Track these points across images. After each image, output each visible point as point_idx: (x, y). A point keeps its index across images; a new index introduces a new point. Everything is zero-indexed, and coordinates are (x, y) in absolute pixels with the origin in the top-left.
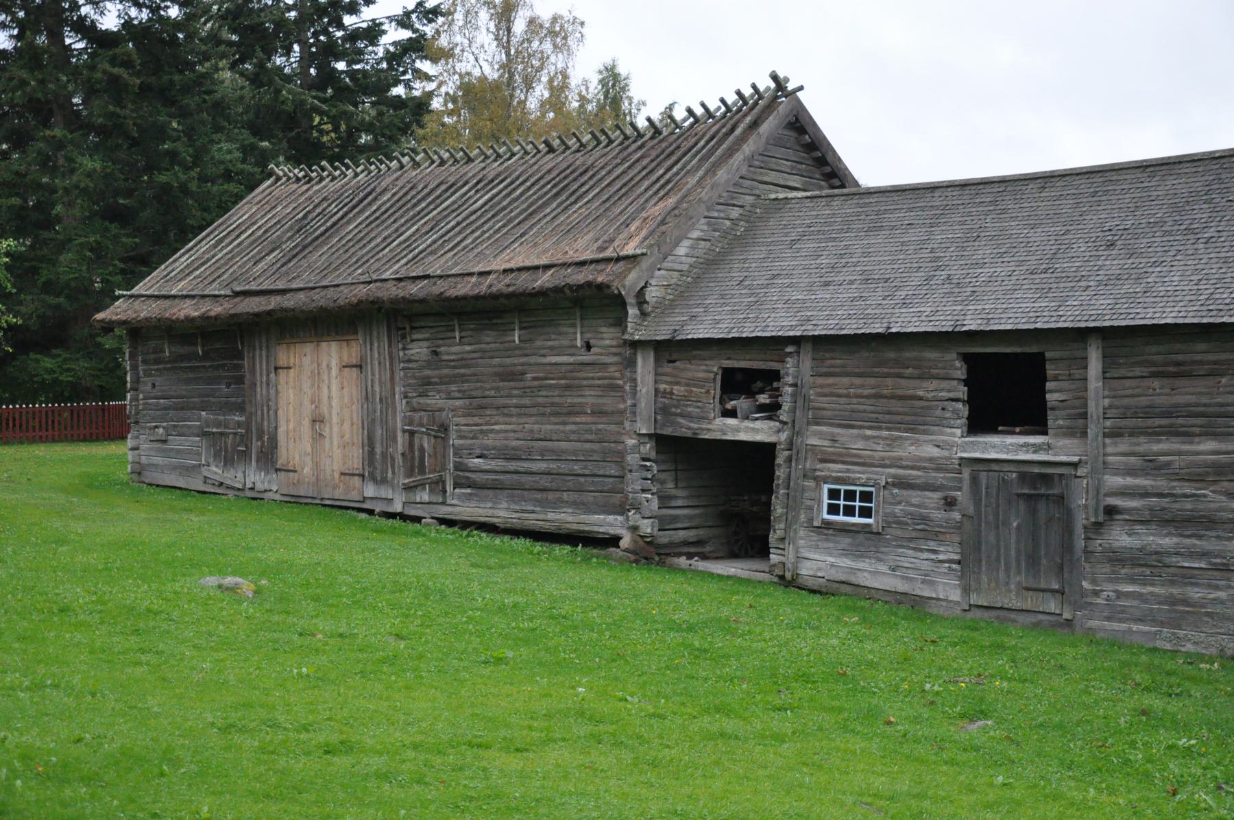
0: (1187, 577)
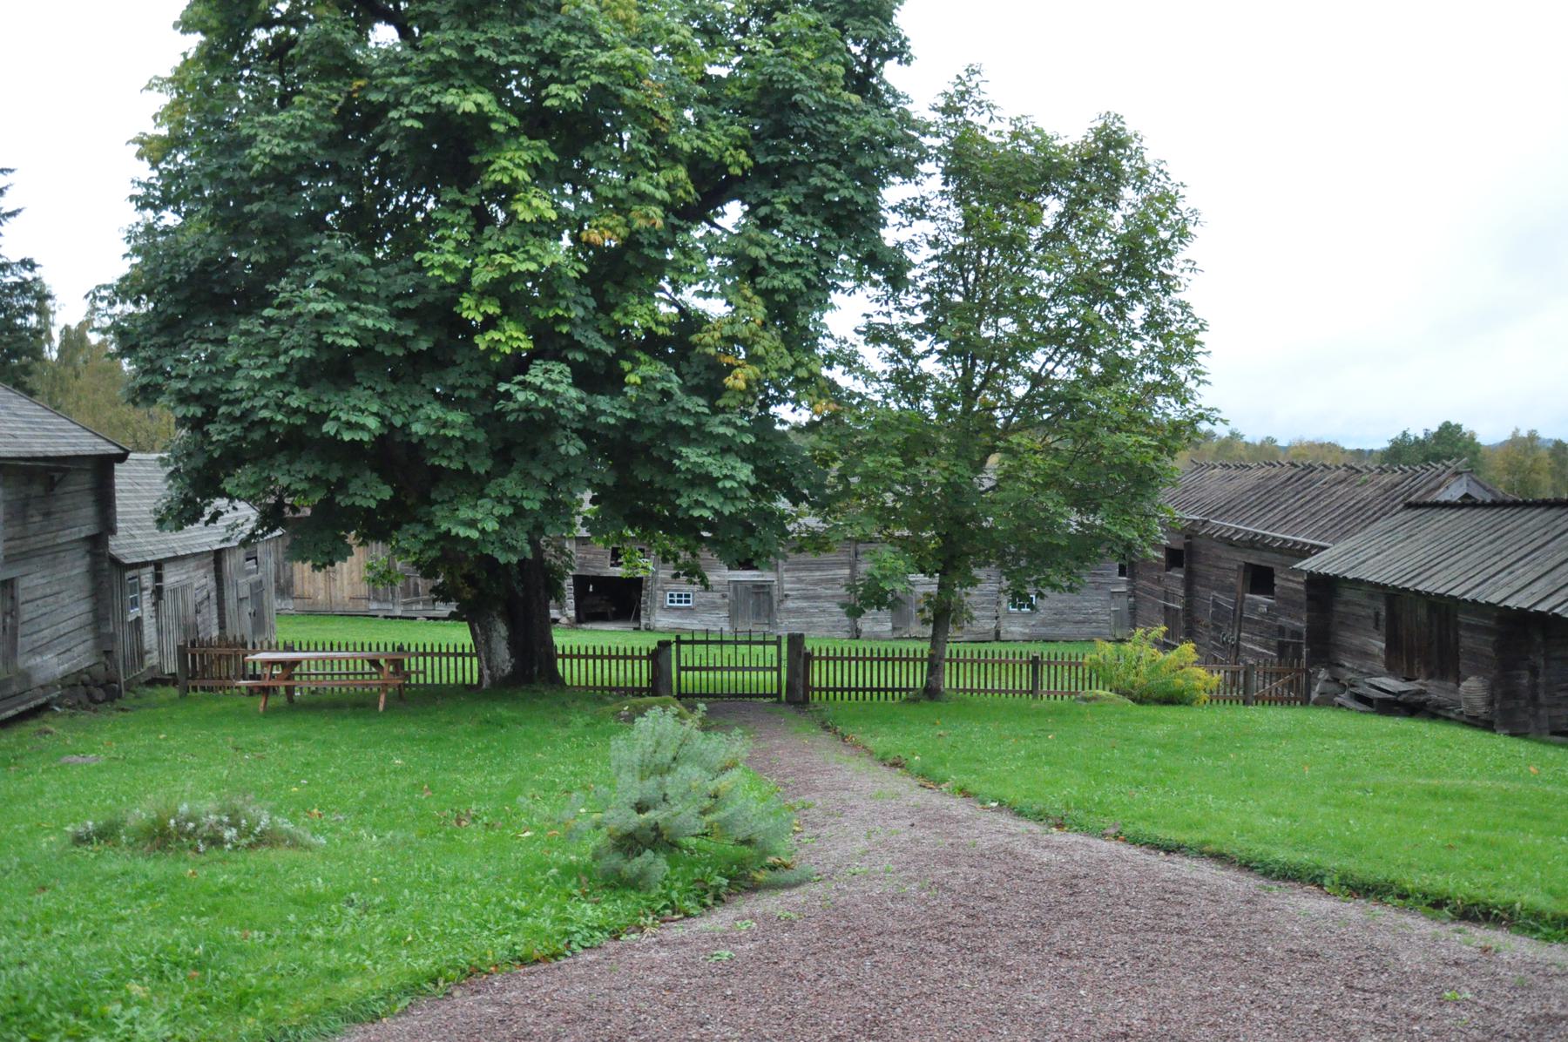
0: (812, 615)
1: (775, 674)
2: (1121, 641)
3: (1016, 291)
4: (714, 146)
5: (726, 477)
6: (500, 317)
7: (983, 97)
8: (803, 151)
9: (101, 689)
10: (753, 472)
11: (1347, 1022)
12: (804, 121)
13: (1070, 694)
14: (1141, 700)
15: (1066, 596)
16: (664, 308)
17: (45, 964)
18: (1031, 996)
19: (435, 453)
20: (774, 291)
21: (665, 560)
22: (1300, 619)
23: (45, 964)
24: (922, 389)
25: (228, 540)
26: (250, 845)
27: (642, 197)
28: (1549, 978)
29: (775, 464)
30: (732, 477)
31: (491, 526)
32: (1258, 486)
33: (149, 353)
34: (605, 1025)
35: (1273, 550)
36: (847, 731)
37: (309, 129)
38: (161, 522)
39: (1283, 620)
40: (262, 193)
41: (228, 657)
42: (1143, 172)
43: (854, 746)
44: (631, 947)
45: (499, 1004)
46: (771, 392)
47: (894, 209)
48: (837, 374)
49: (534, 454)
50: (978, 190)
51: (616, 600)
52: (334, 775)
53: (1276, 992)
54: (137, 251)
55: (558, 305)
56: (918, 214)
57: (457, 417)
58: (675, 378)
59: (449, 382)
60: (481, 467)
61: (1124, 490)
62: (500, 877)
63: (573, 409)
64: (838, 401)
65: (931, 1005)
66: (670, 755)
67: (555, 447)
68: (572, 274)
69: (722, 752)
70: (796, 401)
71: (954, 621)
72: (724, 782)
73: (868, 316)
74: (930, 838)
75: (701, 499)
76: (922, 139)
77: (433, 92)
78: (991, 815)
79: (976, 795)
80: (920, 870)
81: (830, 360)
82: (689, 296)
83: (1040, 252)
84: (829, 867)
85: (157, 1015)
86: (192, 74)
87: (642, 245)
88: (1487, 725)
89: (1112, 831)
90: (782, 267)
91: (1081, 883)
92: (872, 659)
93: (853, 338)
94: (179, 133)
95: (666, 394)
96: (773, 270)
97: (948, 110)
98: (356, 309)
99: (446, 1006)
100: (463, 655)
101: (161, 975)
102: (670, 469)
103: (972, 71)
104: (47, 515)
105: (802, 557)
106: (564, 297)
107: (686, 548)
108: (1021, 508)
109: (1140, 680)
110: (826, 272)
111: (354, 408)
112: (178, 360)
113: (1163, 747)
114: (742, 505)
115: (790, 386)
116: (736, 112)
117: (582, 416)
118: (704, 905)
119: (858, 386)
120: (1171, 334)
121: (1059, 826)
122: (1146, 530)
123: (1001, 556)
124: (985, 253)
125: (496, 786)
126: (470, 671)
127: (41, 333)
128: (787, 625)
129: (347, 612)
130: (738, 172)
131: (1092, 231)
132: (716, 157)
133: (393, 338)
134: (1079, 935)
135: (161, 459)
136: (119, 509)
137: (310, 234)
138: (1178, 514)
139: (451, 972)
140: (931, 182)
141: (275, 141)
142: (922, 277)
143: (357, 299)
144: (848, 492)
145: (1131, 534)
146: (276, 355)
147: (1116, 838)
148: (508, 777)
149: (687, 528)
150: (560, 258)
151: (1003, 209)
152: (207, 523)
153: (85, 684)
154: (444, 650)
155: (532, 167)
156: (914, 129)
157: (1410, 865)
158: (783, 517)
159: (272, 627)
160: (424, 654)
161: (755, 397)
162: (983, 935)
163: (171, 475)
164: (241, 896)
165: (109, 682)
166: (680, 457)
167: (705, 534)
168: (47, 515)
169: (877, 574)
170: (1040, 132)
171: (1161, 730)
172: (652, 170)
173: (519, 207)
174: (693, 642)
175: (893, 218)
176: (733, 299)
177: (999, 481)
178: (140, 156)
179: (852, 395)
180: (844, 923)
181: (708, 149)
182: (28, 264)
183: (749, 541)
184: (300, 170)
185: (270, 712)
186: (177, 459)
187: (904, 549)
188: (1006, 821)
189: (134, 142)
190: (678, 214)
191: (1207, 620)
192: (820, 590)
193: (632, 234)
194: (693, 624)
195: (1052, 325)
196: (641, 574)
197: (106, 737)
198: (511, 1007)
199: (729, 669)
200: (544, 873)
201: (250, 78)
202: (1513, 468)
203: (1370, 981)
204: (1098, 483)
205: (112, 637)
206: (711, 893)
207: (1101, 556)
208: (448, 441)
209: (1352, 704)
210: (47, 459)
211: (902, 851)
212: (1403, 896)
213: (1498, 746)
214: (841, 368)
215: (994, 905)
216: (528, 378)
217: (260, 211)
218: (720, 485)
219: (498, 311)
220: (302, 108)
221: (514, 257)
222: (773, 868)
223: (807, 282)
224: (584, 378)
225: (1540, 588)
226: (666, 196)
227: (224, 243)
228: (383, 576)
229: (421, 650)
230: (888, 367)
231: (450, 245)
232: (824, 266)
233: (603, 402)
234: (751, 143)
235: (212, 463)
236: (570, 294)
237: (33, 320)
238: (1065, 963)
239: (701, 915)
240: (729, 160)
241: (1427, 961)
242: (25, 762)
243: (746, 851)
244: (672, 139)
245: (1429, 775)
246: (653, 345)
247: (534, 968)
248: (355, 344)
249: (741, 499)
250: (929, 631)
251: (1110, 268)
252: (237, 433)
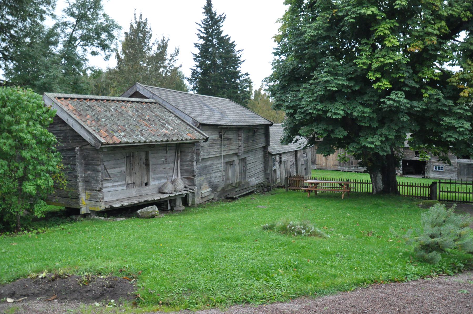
1: (441, 190)
5: (460, 127)
6: (381, 78)
9: (266, 188)
16: (437, 71)
17: (258, 260)
19: (361, 121)
21: (435, 155)
23: (258, 260)
25: (299, 147)
26: (309, 235)
27: (429, 34)
30: (462, 127)
31: (378, 143)
33: (279, 95)
34: (421, 307)
37: (321, 27)
38: (282, 142)
40: (308, 47)
41: (299, 181)
44: (428, 282)
45: (384, 293)
49: (392, 121)
51: (418, 168)
52: (330, 217)
54: (275, 67)
55: (400, 73)
57: (367, 110)
58: (441, 94)
59: (365, 99)
60: (375, 125)
62: (383, 253)
63: (405, 106)
66: (442, 220)
67: (399, 118)
68: (405, 62)
72: (464, 231)
75: (451, 134)
77: (358, 10)
82: (446, 66)
85: (286, 279)
86: (288, 16)
87: (429, 50)
94: (285, 33)
95: (438, 100)
98: (336, 79)
99: (366, 291)
100: (367, 183)
101: (286, 269)
102: (440, 125)
104: (253, 140)
106: (402, 70)
107: (443, 151)
111: (336, 108)
112: (286, 97)
114: (465, 137)
117: (408, 109)
118: (455, 272)
125: (379, 225)
126: (369, 188)
127: (250, 92)
129: (332, 169)
130: (466, 19)
132: (457, 16)
133: (347, 87)
135: (282, 125)
136: (271, 139)
137: (322, 57)
139: (368, 281)
141: (312, 31)
143: (337, 76)
146: (313, 94)
148: (383, 222)
149: (444, 145)
150: (400, 57)
152: (294, 143)
153: (262, 187)
154: (361, 182)
155: (390, 29)
159: (310, 173)
160: (355, 183)
163: (285, 129)
164: (307, 249)
165: (268, 186)
166: (443, 121)
167: (451, 147)
168: (253, 140)
172: (432, 24)
173: (386, 42)
174: (445, 183)
176: (464, 65)
178: (275, 41)
181: (454, 13)
182: (247, 74)
183: (468, 149)
184: (318, 39)
185: (311, 197)
186: (286, 125)
189: (273, 37)
190: (442, 38)
193: (425, 47)
194: (443, 177)
196: (426, 159)
197: (268, 201)
198: (388, 295)
199: (458, 192)
200: (398, 254)
201: (304, 15)
205: (269, 174)
206: (457, 269)
208: (365, 117)
210: (253, 126)
216: (390, 97)
217: (308, 52)
218: (458, 130)
219: (380, 76)
220: (319, 21)
221: (385, 58)
224: (408, 96)
226: (438, 32)
227: (298, 63)
228: (343, 159)
229: (354, 181)
231: (364, 57)
233: (415, 103)
235: (296, 125)
236: (404, 69)
237: (248, 89)
239: (454, 276)
242: (249, 206)
244: (440, 12)
246: (432, 83)
247: (395, 284)
248: (336, 89)
249: (466, 134)
252: (303, 117)
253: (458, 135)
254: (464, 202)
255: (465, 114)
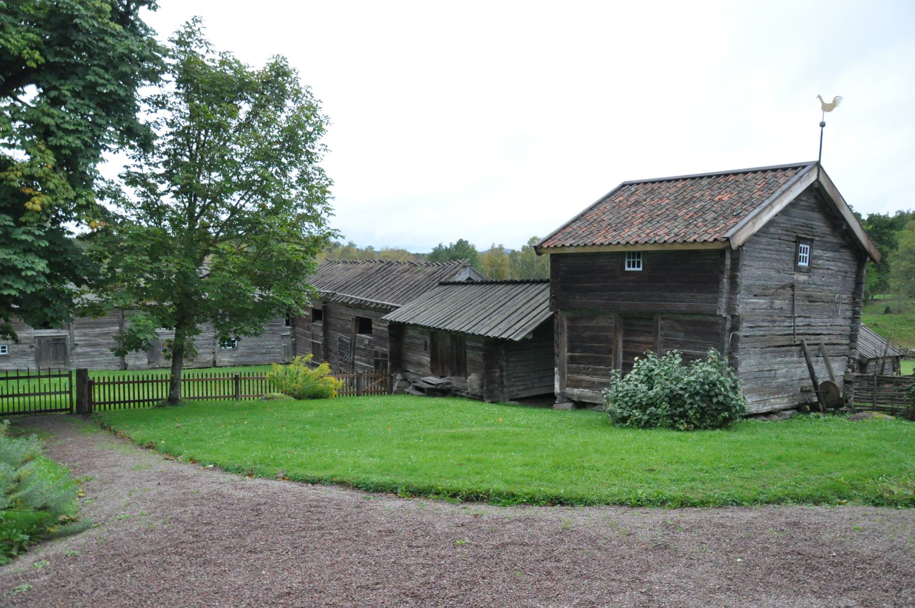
0: (95, 356)
1: (68, 396)
2: (288, 363)
3: (222, 157)
4: (13, 45)
5: (27, 268)
7: (202, 37)
8: (82, 57)
10: (47, 265)
11: (409, 565)
12: (81, 37)
13: (258, 396)
14: (299, 398)
15: (254, 338)
18: (233, 579)
20: (61, 147)
22: (386, 347)
24: (164, 214)
28: (504, 524)
29: (63, 260)
30: (32, 269)
32: (363, 273)
35: (371, 309)
36: (124, 432)
39: (377, 348)
42: (298, 92)
43: (122, 438)
46: (60, 213)
47: (145, 101)
48: (107, 204)
50: (198, 93)
53: (372, 555)
56: (159, 104)
61: (286, 276)
64: (107, 220)
65: (170, 595)
69: (23, 449)
70: (78, 219)
71: (185, 356)
72: (24, 471)
73: (127, 167)
74: (170, 491)
75: (9, 283)
76: (163, 59)
78: (209, 473)
79: (200, 461)
80: (163, 511)
81: (102, 194)
83: (237, 134)
84: (103, 517)
88: (478, 398)
89: (281, 475)
90: (67, 132)
91: (263, 508)
92: (133, 382)
93: (117, 180)
96: (60, 133)
97: (179, 42)
103: (195, 20)
105: (86, 319)
108: (225, 286)
109: (298, 386)
110: (98, 137)
113: (311, 423)
114: (39, 287)
115: (75, 210)
116: (31, 24)
118: (11, 556)
119: (121, 211)
120: (313, 186)
121: (250, 475)
122: (299, 299)
123: (214, 317)
124: (203, 132)
128: (77, 363)
130: (34, 65)
131: (267, 124)
132: (16, 53)
134: (261, 539)
138: (317, 289)
140: (169, 86)
142: (163, 145)
144: (114, 278)
145: (291, 302)
147: (284, 478)
151: (215, 106)
156: (159, 52)
157: (441, 477)
158: (71, 294)
161: (48, 216)
162: (203, 547)
169: (134, 329)
170: (237, 62)
171: (310, 414)
175: (144, 107)
177: (212, 271)
179: (117, 216)
180: (112, 552)
181: (9, 46)
183: (46, 310)
187: (153, 314)
188: (218, 475)
191: (336, 349)
192: (99, 340)
195: (244, 179)
202: (493, 264)
203: (421, 542)
204: (271, 272)
207: (273, 315)
209: (415, 392)
211: (153, 501)
212: (437, 494)
213: (486, 408)
214: (109, 200)
215: (210, 527)
218: (23, 274)
222: (64, 523)
223: (85, 143)
225: (503, 326)
230: (141, 200)
232: (97, 133)
234: (43, 47)
238: (253, 556)
239: (8, 563)
240: (26, 56)
241: (448, 527)
243: (43, 514)
245: (452, 427)
249: (39, 282)
250: (170, 363)
251: (278, 146)
253: (24, 283)
254: (46, 411)
255: (36, 244)
